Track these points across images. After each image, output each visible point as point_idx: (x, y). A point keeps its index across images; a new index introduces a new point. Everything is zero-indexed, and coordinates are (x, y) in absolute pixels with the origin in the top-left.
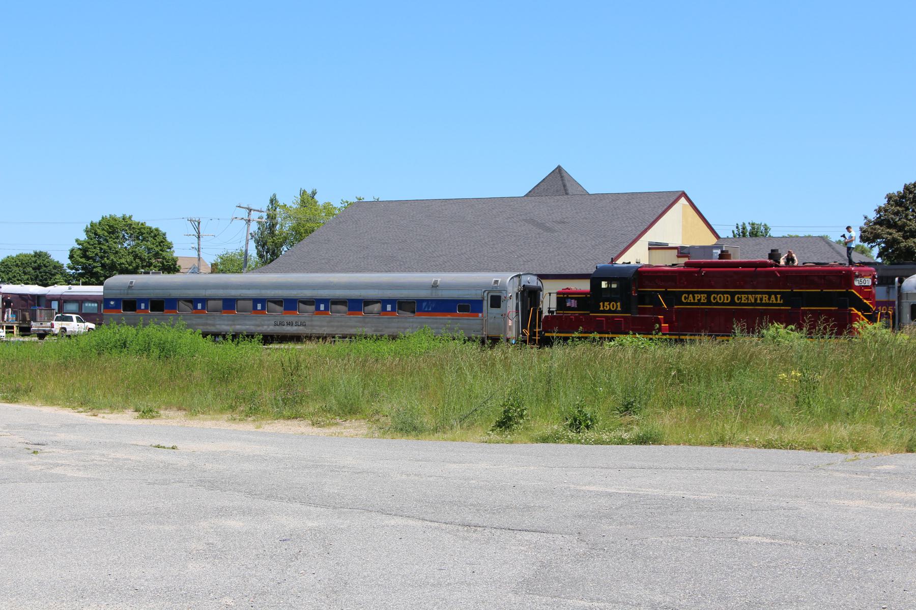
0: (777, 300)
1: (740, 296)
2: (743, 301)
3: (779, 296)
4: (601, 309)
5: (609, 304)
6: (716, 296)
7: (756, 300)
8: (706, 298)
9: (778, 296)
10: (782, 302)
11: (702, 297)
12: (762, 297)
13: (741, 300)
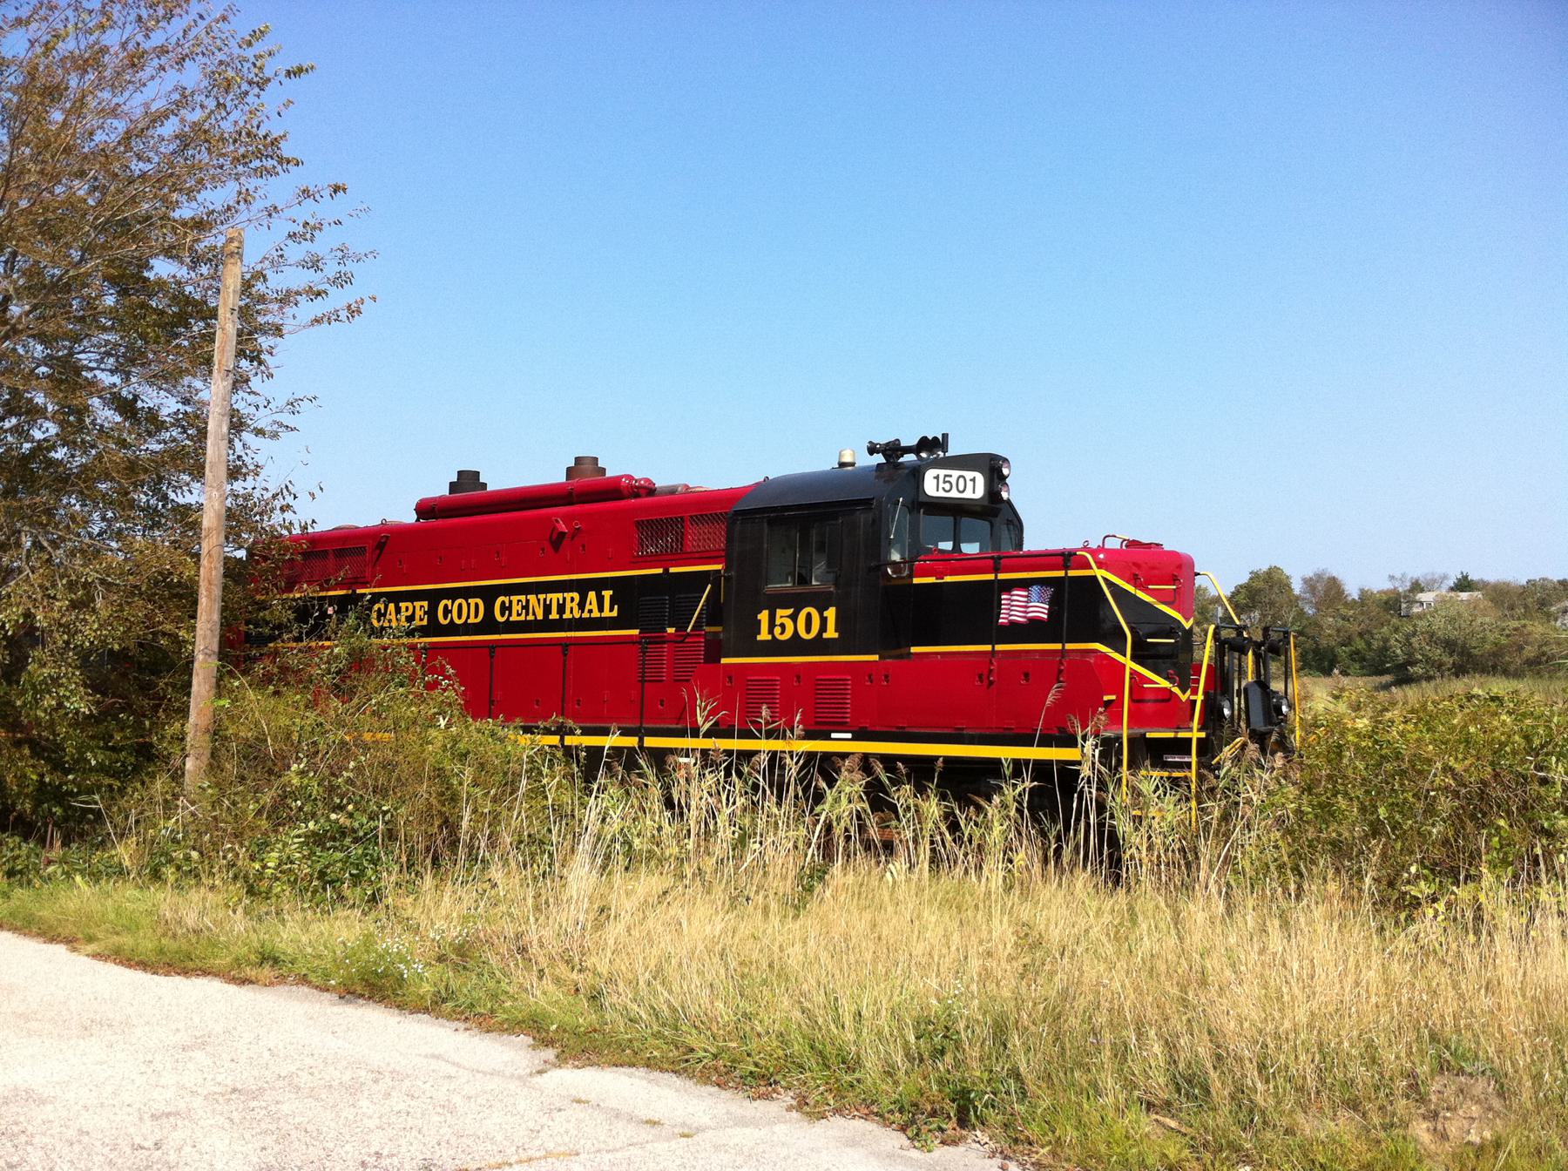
0: (601, 609)
1: (506, 599)
2: (514, 618)
3: (607, 594)
4: (764, 636)
5: (794, 618)
6: (449, 603)
7: (547, 609)
8: (425, 613)
9: (604, 593)
10: (615, 614)
11: (418, 608)
12: (564, 599)
13: (510, 615)
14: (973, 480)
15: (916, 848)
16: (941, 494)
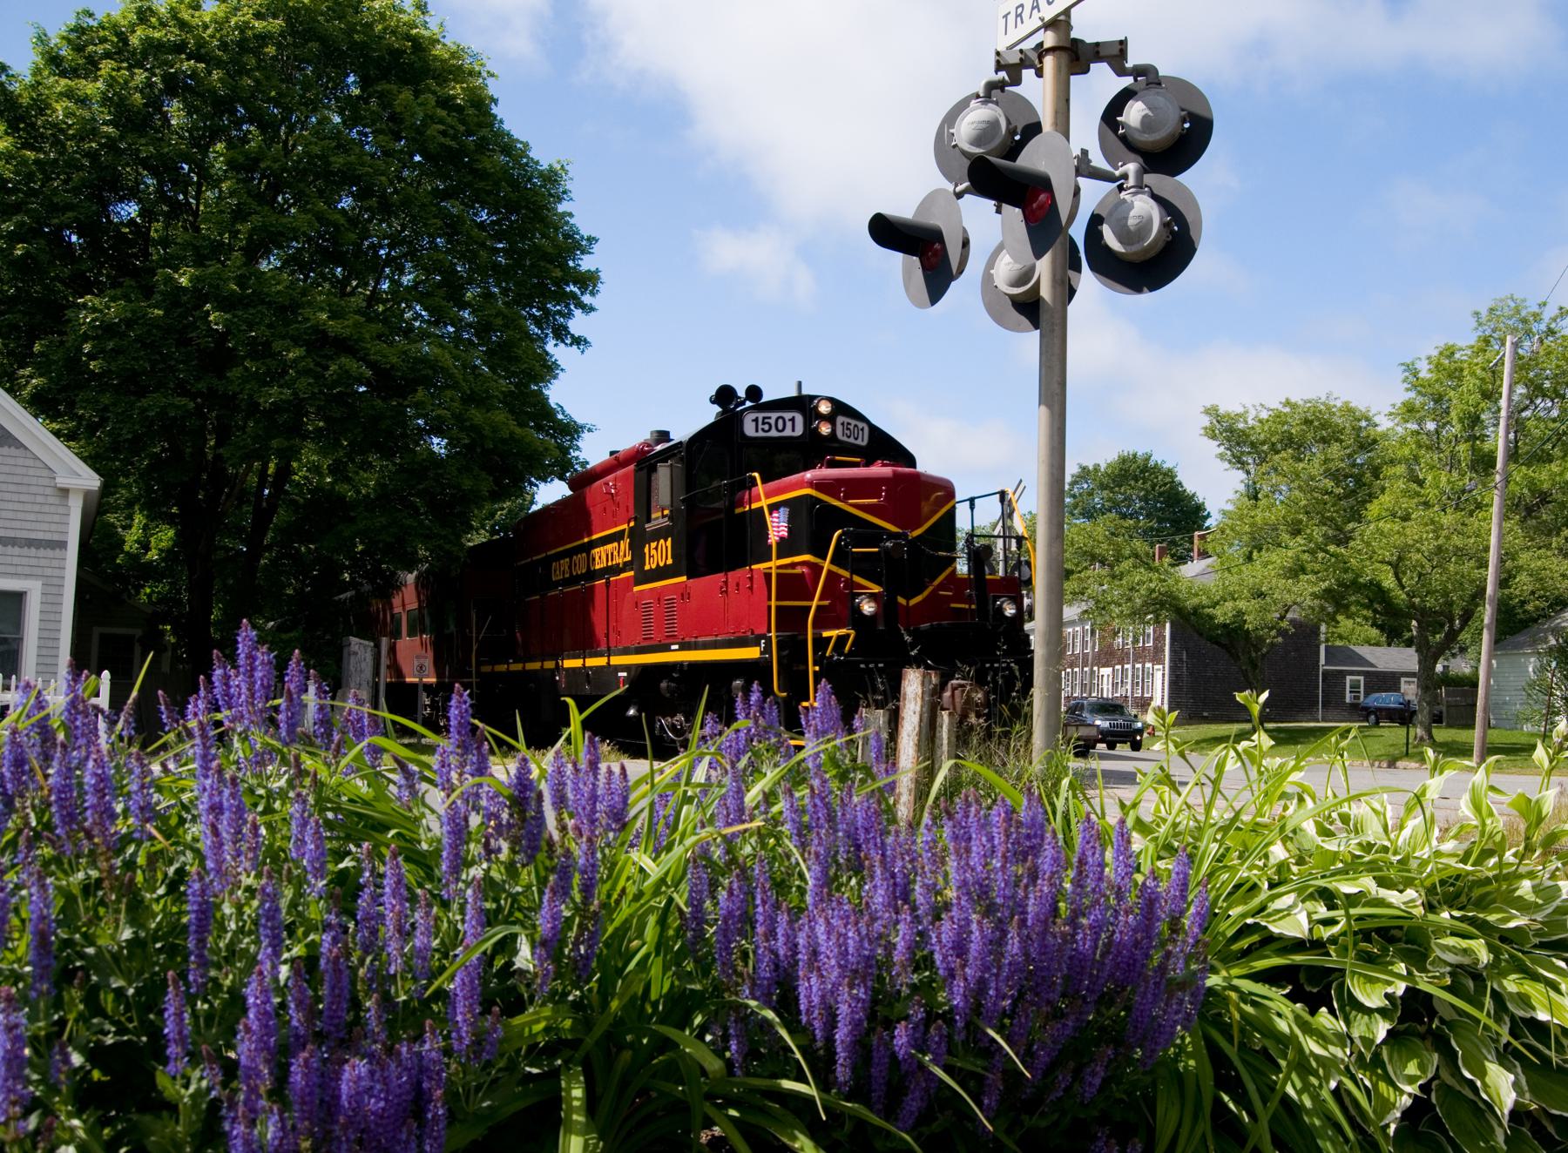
14: (793, 420)
15: (1180, 1125)
16: (761, 434)
